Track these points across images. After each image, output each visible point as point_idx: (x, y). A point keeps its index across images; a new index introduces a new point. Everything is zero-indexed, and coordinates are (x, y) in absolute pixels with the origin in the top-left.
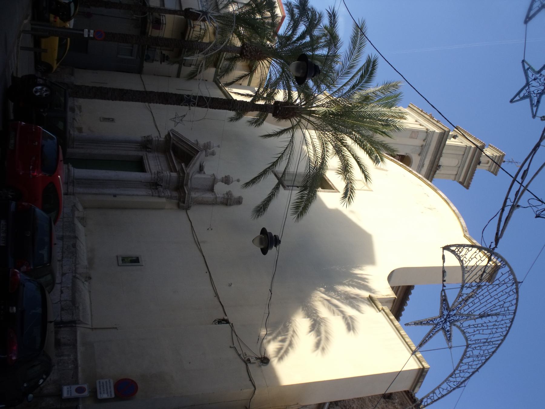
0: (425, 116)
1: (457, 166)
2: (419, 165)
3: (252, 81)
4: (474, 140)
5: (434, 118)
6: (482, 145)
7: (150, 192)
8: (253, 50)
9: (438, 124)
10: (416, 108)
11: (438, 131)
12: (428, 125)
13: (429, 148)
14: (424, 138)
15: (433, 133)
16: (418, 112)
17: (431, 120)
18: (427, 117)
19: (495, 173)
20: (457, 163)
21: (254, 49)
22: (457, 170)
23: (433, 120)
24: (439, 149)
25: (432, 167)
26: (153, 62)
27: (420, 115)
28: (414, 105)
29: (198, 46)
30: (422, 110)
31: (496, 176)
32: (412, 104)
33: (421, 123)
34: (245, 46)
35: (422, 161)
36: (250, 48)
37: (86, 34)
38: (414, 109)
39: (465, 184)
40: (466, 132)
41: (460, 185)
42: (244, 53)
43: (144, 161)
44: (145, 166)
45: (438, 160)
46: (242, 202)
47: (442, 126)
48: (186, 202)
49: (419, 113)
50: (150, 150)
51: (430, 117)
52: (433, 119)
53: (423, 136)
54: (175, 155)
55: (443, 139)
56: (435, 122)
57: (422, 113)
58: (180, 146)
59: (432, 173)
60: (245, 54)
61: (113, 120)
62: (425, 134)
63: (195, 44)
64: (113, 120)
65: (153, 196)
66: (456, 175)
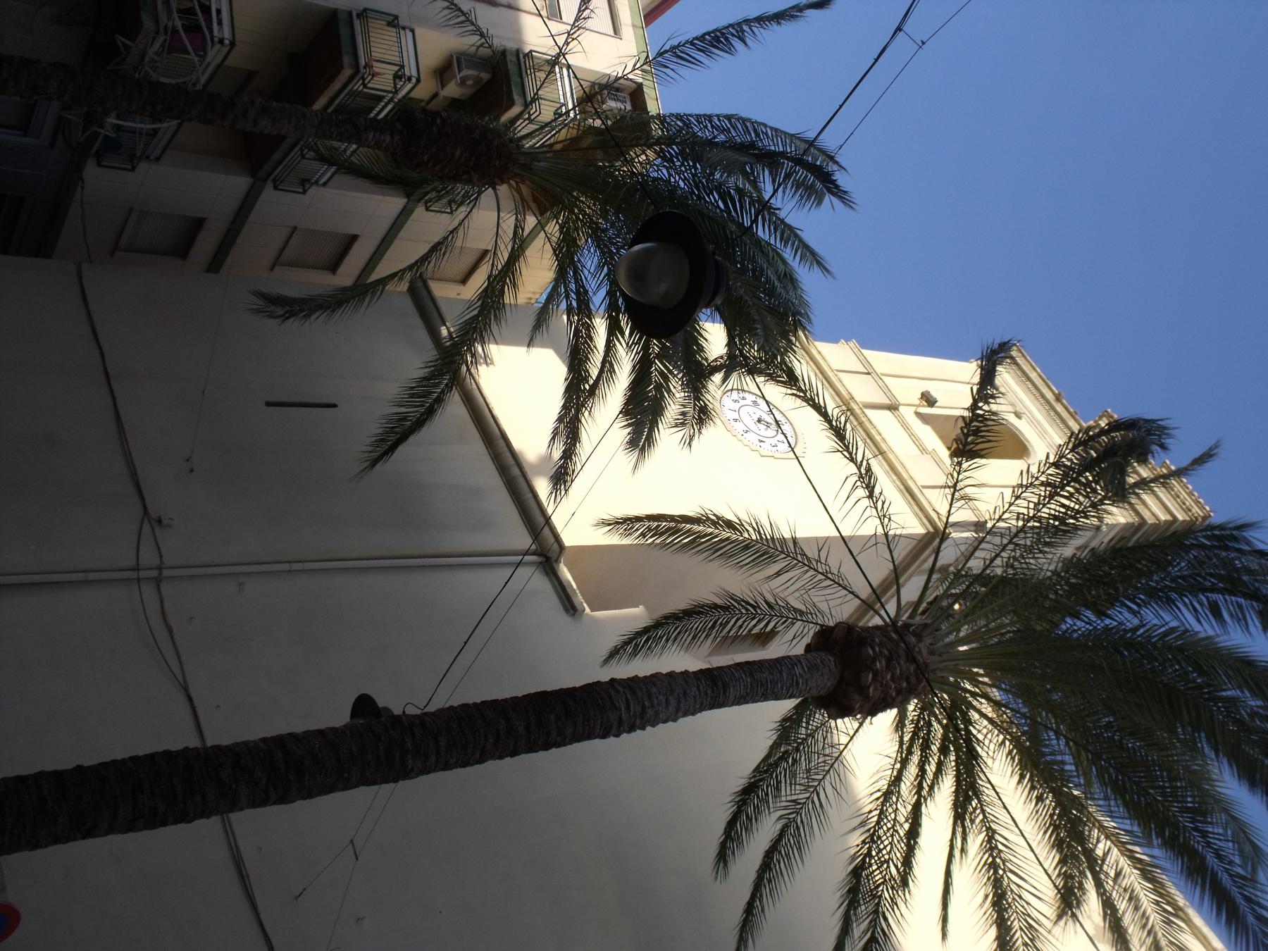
3: (239, 241)
4: (1180, 509)
6: (1188, 519)
16: (1043, 396)
27: (1052, 413)
28: (1028, 358)
30: (1059, 394)
38: (1029, 379)
57: (1059, 408)
61: (335, 406)
64: (335, 406)
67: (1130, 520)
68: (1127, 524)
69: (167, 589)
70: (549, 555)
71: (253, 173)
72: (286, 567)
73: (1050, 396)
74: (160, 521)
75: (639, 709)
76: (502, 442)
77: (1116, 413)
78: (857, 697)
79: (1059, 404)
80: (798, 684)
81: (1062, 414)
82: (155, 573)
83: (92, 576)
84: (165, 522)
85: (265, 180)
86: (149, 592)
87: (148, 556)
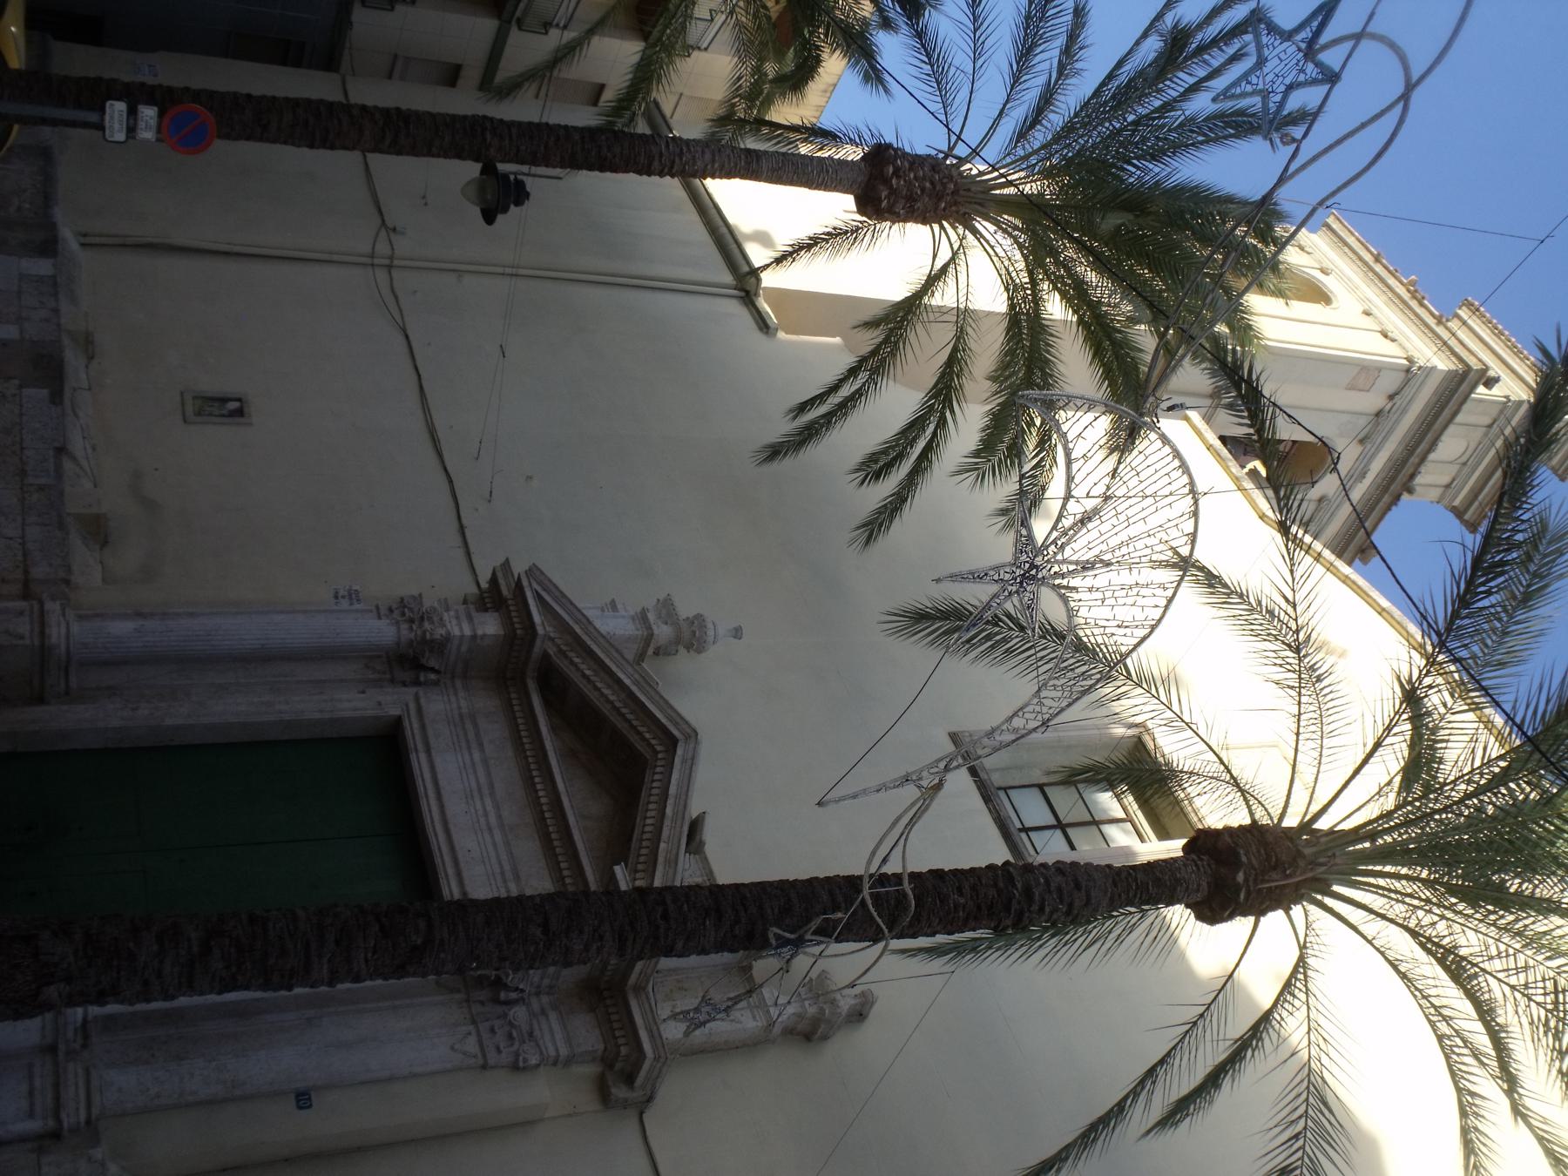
0: (1392, 281)
1: (1460, 461)
2: (1352, 471)
5: (1426, 302)
7: (471, 1045)
8: (923, 190)
9: (1440, 330)
10: (1353, 239)
11: (1443, 364)
12: (1412, 336)
13: (1397, 422)
14: (1392, 390)
15: (1428, 374)
16: (1361, 259)
17: (1414, 304)
18: (1397, 290)
19: (1560, 472)
20: (1462, 450)
21: (928, 185)
22: (1453, 474)
23: (1423, 310)
24: (1430, 425)
25: (1393, 479)
26: (392, 9)
27: (1370, 274)
28: (1346, 223)
29: (674, 162)
30: (1379, 254)
31: (1561, 483)
32: (1338, 219)
33: (1389, 328)
34: (891, 170)
35: (1366, 460)
36: (912, 176)
37: (116, 126)
38: (1346, 244)
39: (1467, 517)
40: (1503, 335)
41: (1451, 516)
42: (880, 201)
43: (413, 757)
44: (423, 802)
45: (1417, 460)
46: (868, 1014)
47: (1459, 345)
48: (639, 1081)
49: (1366, 263)
50: (433, 676)
51: (1409, 291)
52: (1422, 305)
53: (1389, 383)
54: (547, 704)
55: (1453, 395)
56: (1431, 322)
57: (1378, 268)
58: (581, 683)
59: (1387, 498)
60: (884, 204)
62: (1403, 375)
63: (661, 155)
65: (484, 1067)
66: (1448, 486)
67: (1453, 367)
68: (1449, 372)
69: (395, 273)
70: (748, 289)
71: (499, 17)
72: (500, 270)
73: (1368, 258)
74: (394, 230)
75: (678, 150)
76: (714, 211)
77: (1476, 300)
78: (882, 188)
79: (1379, 265)
80: (828, 171)
81: (1462, 355)
82: (387, 262)
83: (335, 258)
84: (398, 229)
85: (509, 22)
86: (381, 275)
87: (382, 248)
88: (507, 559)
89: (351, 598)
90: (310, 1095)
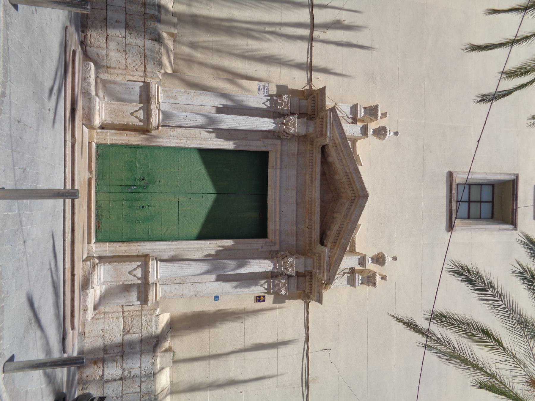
88: (325, 87)
89: (264, 91)
90: (218, 296)
